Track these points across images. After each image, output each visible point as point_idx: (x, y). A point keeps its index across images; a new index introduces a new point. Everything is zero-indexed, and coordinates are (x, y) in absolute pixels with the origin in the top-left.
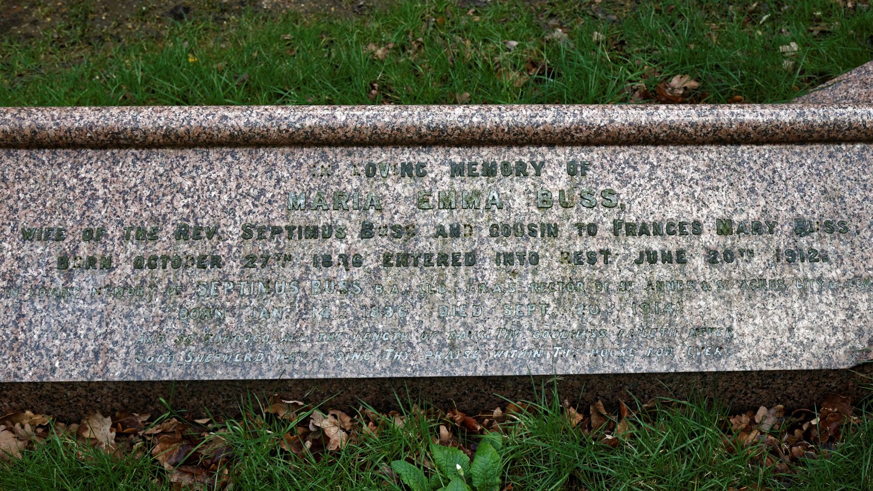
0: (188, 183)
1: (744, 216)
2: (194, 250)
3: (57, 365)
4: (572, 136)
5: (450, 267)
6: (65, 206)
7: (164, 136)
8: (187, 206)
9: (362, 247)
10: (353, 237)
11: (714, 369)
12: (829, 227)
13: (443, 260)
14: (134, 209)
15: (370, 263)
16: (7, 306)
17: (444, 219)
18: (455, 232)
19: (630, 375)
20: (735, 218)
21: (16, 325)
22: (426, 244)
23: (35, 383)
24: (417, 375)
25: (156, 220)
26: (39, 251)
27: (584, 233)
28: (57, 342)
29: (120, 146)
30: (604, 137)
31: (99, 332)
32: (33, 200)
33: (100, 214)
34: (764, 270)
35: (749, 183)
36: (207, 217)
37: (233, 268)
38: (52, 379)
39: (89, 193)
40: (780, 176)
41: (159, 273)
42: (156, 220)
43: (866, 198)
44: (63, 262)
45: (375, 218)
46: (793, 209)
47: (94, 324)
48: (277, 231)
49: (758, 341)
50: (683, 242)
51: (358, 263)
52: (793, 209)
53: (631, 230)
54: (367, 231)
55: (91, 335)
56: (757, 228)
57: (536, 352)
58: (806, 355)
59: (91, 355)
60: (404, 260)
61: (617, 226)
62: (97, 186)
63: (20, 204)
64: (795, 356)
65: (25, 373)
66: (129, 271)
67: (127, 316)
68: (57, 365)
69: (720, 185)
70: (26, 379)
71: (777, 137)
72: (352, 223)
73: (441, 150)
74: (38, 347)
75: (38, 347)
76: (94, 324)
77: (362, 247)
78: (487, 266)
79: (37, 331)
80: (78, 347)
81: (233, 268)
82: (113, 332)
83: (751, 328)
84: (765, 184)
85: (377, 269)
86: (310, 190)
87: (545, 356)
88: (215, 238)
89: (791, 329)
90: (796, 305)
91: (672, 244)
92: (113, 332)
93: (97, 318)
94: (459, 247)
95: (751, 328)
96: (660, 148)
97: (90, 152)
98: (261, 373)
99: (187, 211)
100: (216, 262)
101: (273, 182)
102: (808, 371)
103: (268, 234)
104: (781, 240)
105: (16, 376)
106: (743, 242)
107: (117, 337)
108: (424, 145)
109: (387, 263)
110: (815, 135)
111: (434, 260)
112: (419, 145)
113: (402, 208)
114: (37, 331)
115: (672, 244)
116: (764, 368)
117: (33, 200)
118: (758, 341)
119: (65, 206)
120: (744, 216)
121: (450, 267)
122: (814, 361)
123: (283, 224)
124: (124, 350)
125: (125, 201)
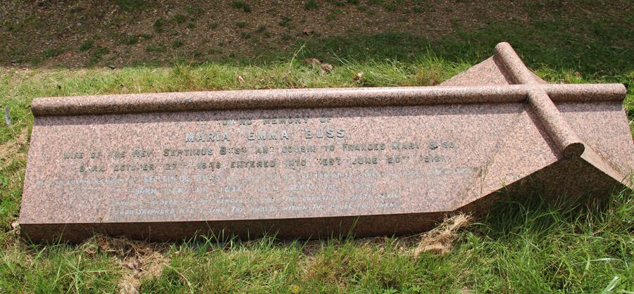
0: (139, 130)
1: (405, 140)
2: (142, 161)
3: (80, 215)
4: (322, 103)
5: (263, 167)
6: (84, 142)
7: (128, 108)
8: (139, 141)
9: (220, 158)
10: (216, 153)
11: (389, 213)
12: (445, 145)
13: (259, 165)
14: (114, 143)
15: (224, 166)
16: (244, 150)
17: (261, 145)
18: (265, 152)
19: (349, 217)
20: (401, 141)
21: (61, 197)
22: (253, 157)
23: (71, 224)
24: (247, 219)
25: (125, 148)
26: (72, 163)
27: (328, 150)
28: (80, 205)
29: (108, 114)
30: (337, 103)
31: (99, 200)
32: (69, 139)
33: (98, 144)
34: (414, 165)
35: (408, 124)
36: (148, 146)
37: (160, 169)
38: (78, 222)
39: (94, 136)
40: (423, 121)
41: (126, 172)
42: (125, 148)
43: (463, 131)
44: (82, 169)
45: (226, 144)
46: (428, 137)
47: (96, 196)
48: (180, 152)
49: (411, 199)
50: (376, 153)
51: (218, 166)
52: (428, 137)
53: (351, 148)
54: (223, 151)
55: (95, 201)
56: (411, 147)
57: (304, 207)
58: (433, 205)
59: (95, 211)
60: (242, 164)
61: (345, 146)
62: (98, 132)
63: (63, 142)
64: (428, 206)
65: (66, 219)
66: (112, 172)
67: (112, 192)
68: (80, 215)
69: (394, 125)
70: (67, 222)
71: (420, 102)
72: (216, 148)
73: (259, 111)
74: (71, 207)
75: (71, 207)
76: (96, 196)
77: (220, 158)
78: (281, 166)
79: (71, 200)
80: (90, 207)
81: (160, 169)
82: (105, 200)
83: (408, 193)
84: (415, 125)
85: (228, 169)
86: (196, 132)
87: (308, 209)
88: (151, 156)
89: (427, 194)
90: (429, 182)
91: (370, 155)
92: (105, 200)
93: (97, 194)
94: (268, 158)
95: (408, 193)
96: (365, 108)
97: (95, 117)
98: (173, 219)
99: (138, 143)
100: (152, 167)
101: (179, 128)
102: (434, 213)
103: (176, 154)
104: (423, 152)
105: (62, 221)
106: (404, 152)
107: (107, 203)
108: (251, 109)
109: (232, 167)
110: (439, 101)
111: (255, 164)
112: (248, 109)
113: (239, 140)
114: (71, 200)
115: (370, 155)
116: (413, 212)
117: (69, 139)
118: (411, 199)
119: (84, 142)
120: (405, 140)
121: (263, 167)
122: (437, 208)
123: (183, 149)
124: (110, 209)
125: (110, 139)
